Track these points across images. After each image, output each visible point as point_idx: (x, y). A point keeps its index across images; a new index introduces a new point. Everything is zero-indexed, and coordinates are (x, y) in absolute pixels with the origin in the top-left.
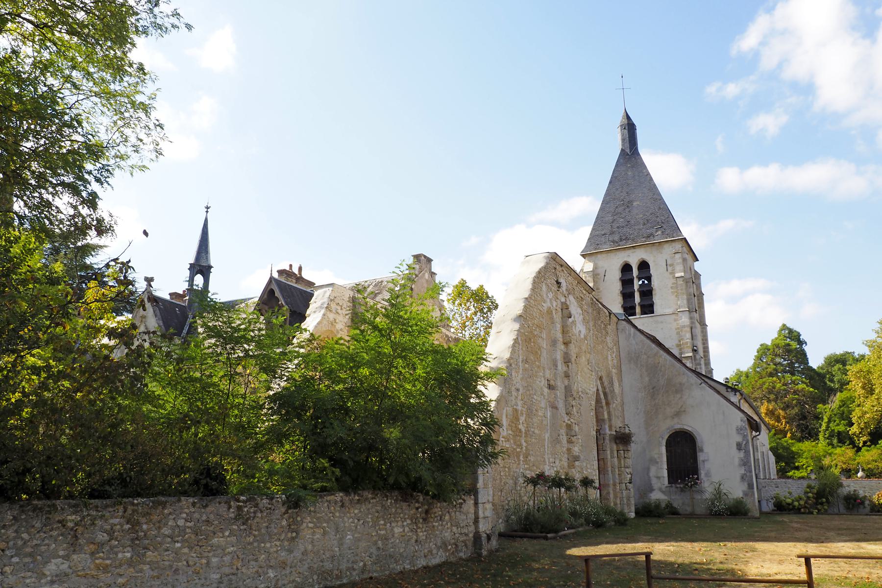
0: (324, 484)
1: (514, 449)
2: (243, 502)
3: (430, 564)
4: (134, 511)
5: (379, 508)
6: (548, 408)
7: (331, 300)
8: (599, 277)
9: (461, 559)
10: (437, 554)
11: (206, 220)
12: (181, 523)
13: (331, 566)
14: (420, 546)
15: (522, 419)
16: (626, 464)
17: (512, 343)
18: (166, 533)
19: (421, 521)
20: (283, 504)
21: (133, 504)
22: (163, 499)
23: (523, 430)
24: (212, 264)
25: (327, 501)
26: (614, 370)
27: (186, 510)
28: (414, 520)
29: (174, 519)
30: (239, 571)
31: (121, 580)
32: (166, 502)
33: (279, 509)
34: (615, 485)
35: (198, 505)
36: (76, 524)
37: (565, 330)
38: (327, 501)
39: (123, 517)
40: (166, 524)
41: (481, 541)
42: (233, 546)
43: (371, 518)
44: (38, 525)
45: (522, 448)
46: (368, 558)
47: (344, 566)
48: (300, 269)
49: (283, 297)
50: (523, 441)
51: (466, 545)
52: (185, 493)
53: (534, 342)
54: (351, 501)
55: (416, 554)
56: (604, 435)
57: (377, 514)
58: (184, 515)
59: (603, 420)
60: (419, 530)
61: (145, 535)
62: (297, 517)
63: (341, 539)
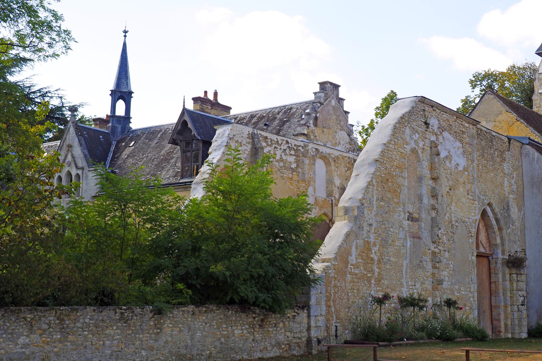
0: (180, 300)
1: (365, 274)
2: (124, 310)
3: (265, 357)
4: (60, 313)
5: (222, 317)
6: (408, 239)
7: (230, 139)
9: (294, 355)
10: (272, 350)
11: (125, 45)
12: (87, 320)
13: (185, 352)
14: (256, 343)
15: (375, 249)
16: (519, 287)
17: (365, 185)
18: (79, 326)
19: (258, 326)
20: (151, 312)
21: (60, 310)
22: (76, 307)
23: (376, 258)
24: (133, 90)
25: (182, 311)
26: (511, 196)
27: (90, 314)
28: (252, 326)
29: (83, 318)
30: (123, 350)
31: (55, 350)
32: (78, 309)
33: (148, 314)
34: (506, 306)
35: (96, 311)
36: (32, 319)
37: (433, 166)
38: (182, 311)
39: (55, 316)
40: (79, 321)
41: (312, 343)
42: (119, 335)
43: (216, 323)
44: (13, 319)
45: (374, 273)
46: (213, 349)
47: (195, 352)
48: (216, 94)
49: (196, 129)
50: (375, 267)
51: (299, 346)
52: (90, 305)
53: (392, 182)
54: (200, 311)
55: (253, 349)
56: (496, 259)
57: (220, 321)
58: (89, 317)
59: (496, 245)
60: (255, 333)
61: (67, 326)
62: (160, 320)
63: (192, 335)
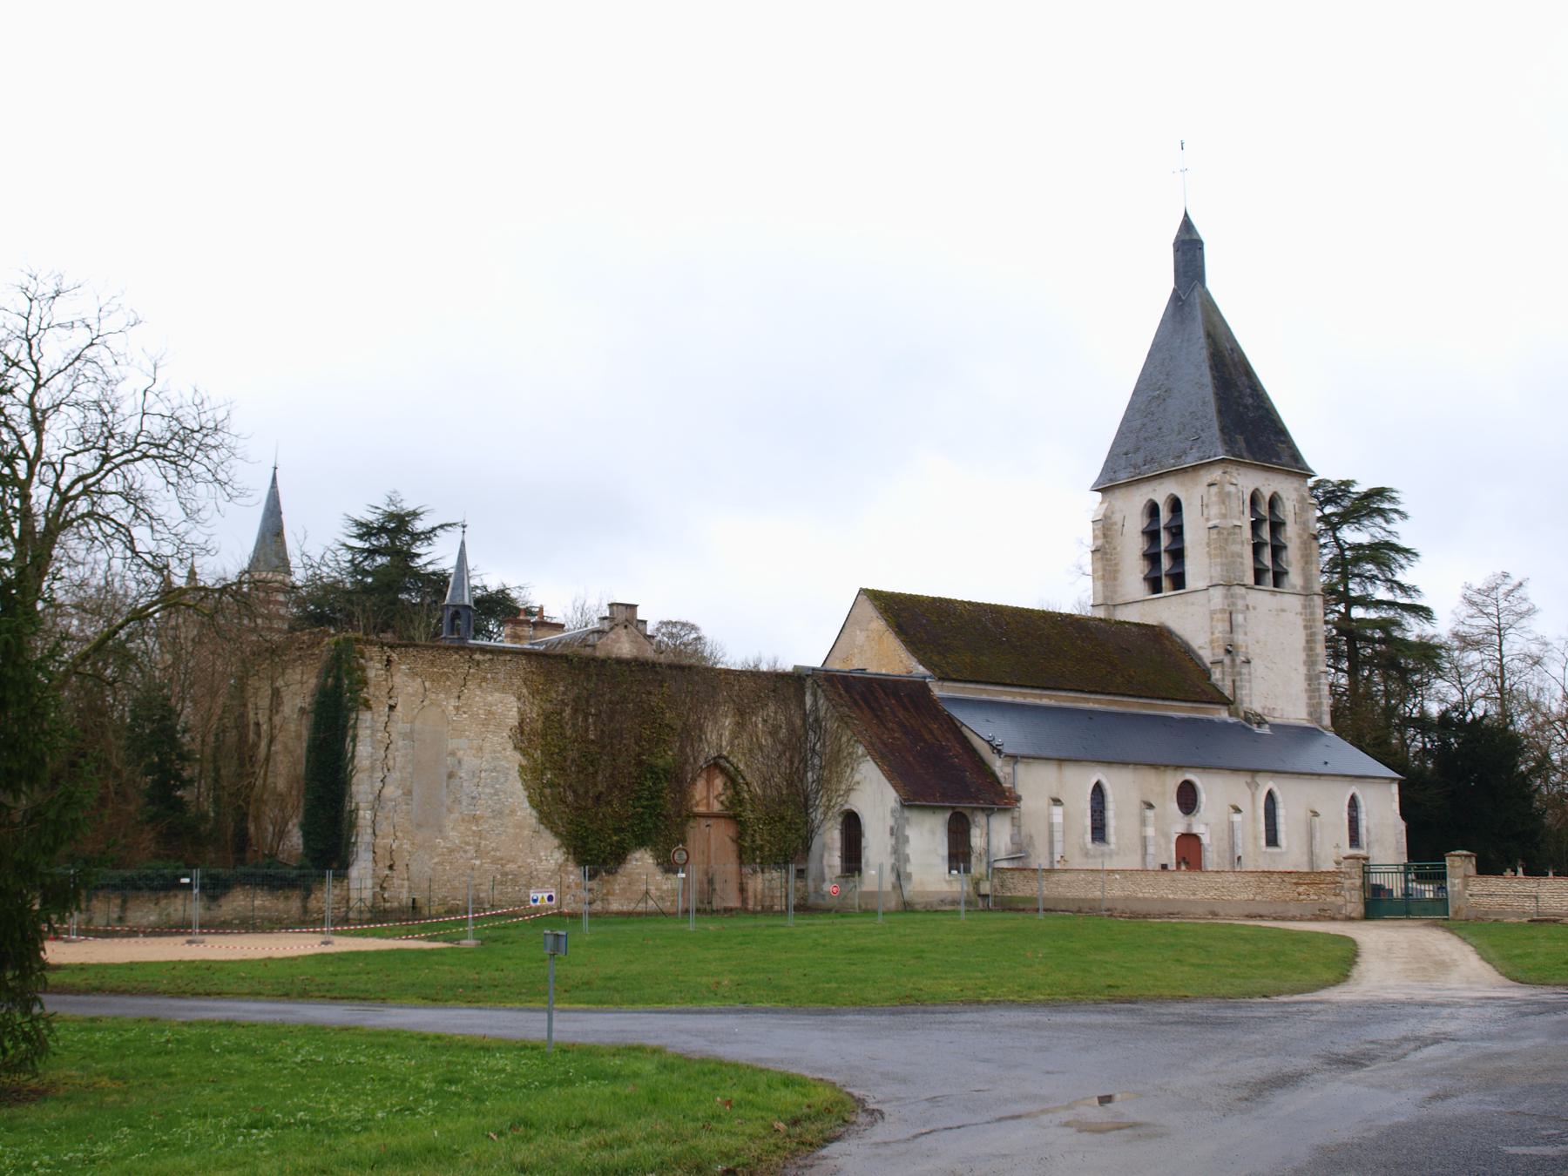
8: (1116, 527)
